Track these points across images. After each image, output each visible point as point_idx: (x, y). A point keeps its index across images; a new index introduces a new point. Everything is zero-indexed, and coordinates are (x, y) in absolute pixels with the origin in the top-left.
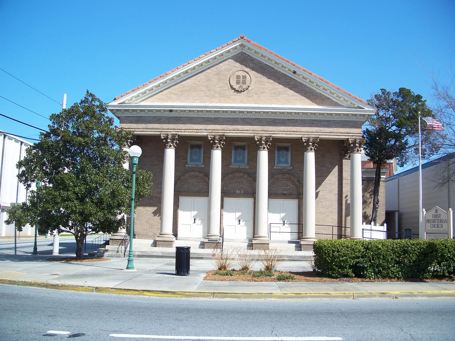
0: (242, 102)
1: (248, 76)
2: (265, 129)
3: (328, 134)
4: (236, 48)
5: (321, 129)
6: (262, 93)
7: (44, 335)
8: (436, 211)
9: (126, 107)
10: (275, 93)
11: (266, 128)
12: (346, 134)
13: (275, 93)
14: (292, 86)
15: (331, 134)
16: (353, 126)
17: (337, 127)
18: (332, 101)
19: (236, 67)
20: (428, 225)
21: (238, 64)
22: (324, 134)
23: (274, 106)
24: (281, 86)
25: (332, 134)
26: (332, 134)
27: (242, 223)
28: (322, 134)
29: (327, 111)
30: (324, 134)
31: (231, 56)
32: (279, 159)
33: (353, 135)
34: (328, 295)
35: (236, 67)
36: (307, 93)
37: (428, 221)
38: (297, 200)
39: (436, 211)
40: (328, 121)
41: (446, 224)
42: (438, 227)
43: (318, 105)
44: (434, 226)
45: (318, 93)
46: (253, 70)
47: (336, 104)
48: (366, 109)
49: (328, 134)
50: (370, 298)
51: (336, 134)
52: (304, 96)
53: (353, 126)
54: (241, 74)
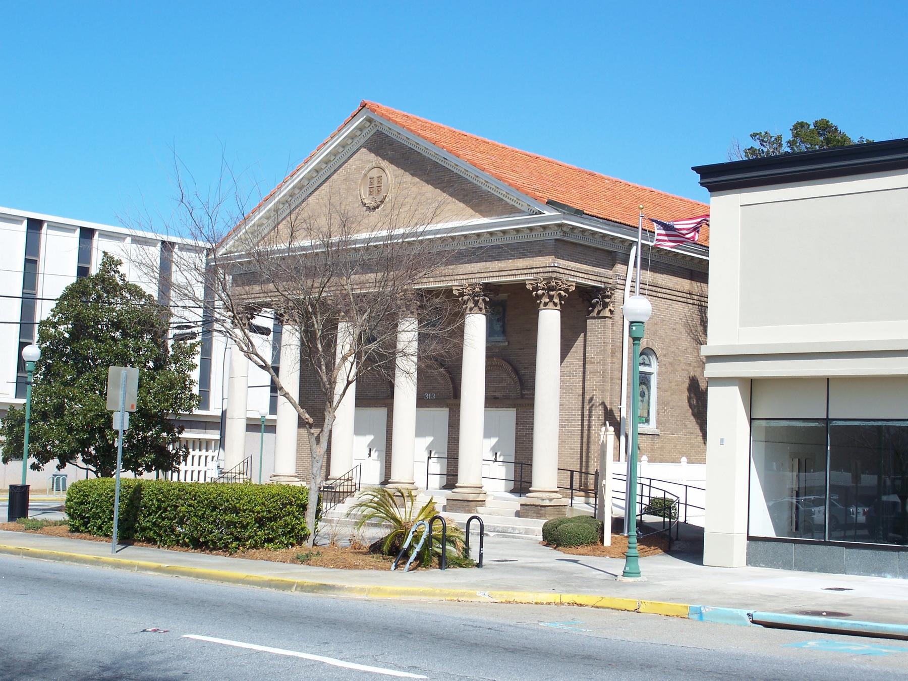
1: (384, 175)
3: (498, 274)
4: (360, 128)
5: (488, 264)
12: (526, 271)
14: (445, 185)
15: (501, 273)
16: (540, 252)
18: (507, 203)
22: (491, 274)
24: (430, 187)
25: (504, 273)
26: (504, 273)
27: (374, 454)
28: (488, 274)
29: (502, 226)
30: (491, 274)
31: (362, 141)
32: (24, 410)
33: (538, 270)
34: (379, 590)
36: (467, 195)
38: (448, 409)
40: (498, 247)
43: (484, 214)
45: (484, 192)
46: (392, 163)
47: (513, 210)
48: (547, 213)
49: (498, 274)
51: (510, 273)
52: (464, 202)
53: (540, 252)
54: (375, 173)
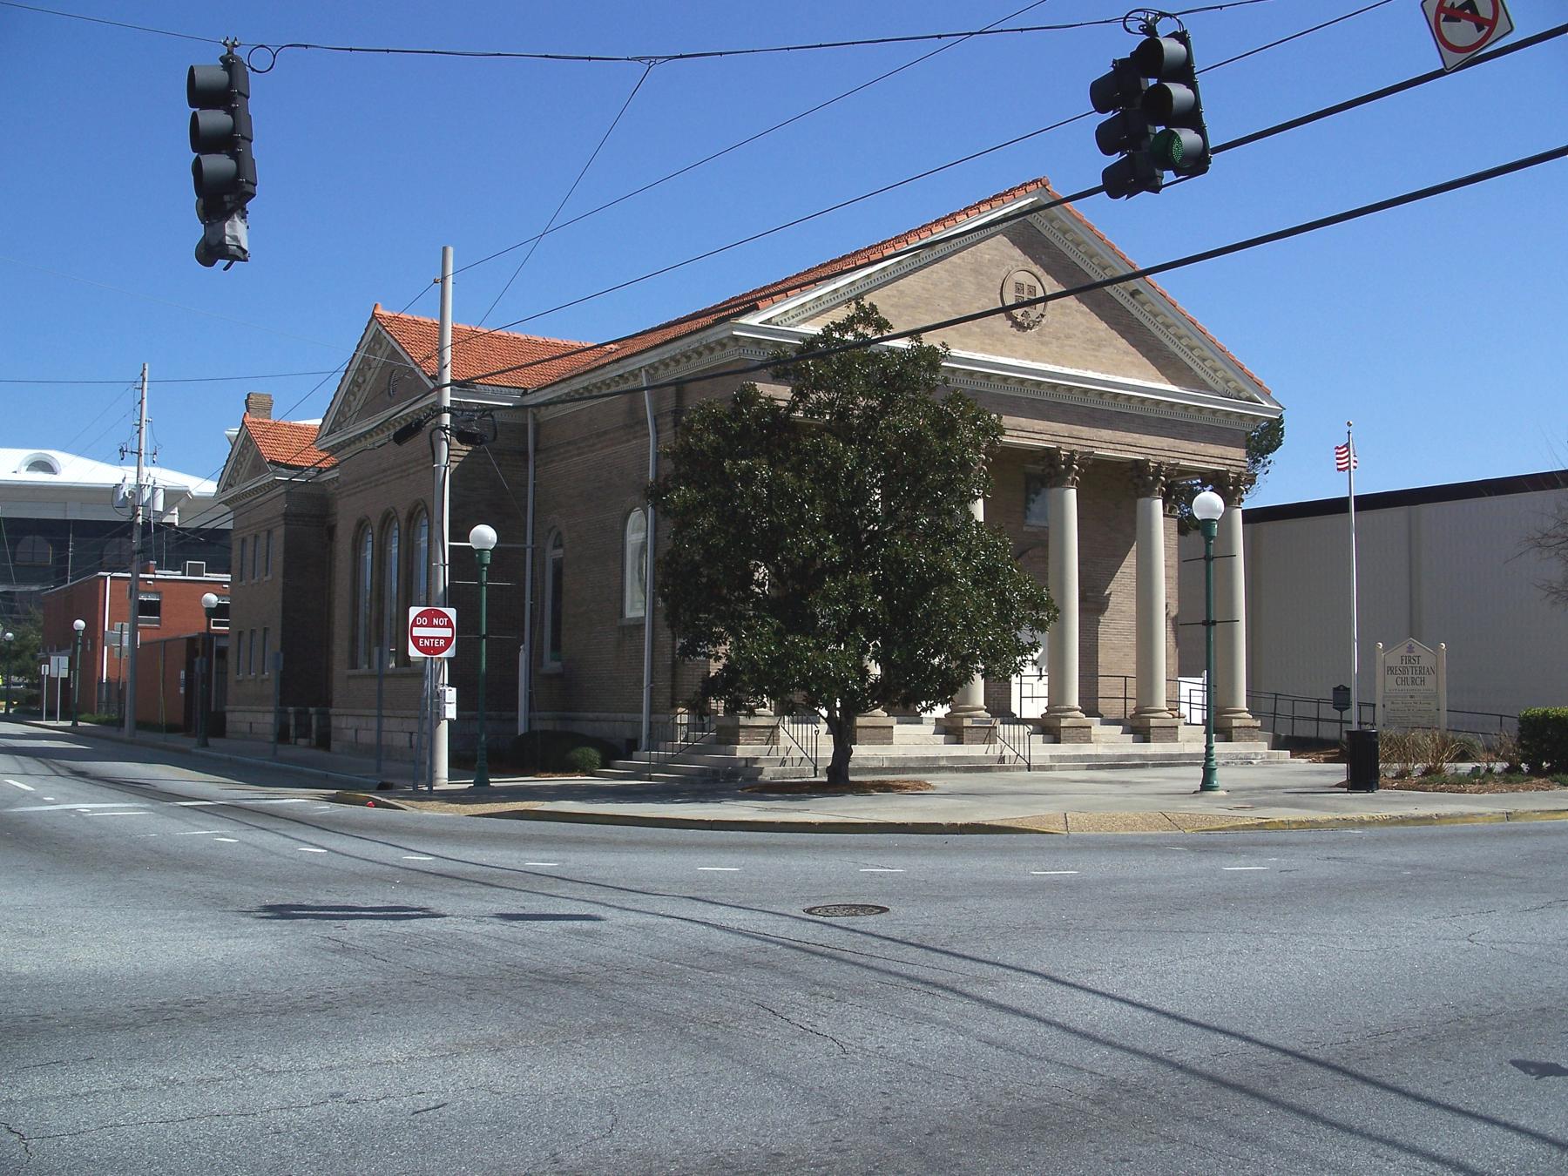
0: (1027, 356)
2: (1075, 433)
6: (1068, 337)
7: (1514, 1063)
8: (1410, 649)
9: (781, 336)
10: (1091, 341)
11: (1078, 430)
13: (1091, 341)
17: (552, 639)
18: (1197, 376)
19: (1012, 258)
20: (1391, 678)
21: (1017, 252)
23: (1090, 374)
35: (1012, 258)
37: (1391, 670)
39: (1410, 649)
41: (1433, 676)
42: (1414, 682)
44: (1405, 681)
47: (1203, 386)
50: (1206, 863)
